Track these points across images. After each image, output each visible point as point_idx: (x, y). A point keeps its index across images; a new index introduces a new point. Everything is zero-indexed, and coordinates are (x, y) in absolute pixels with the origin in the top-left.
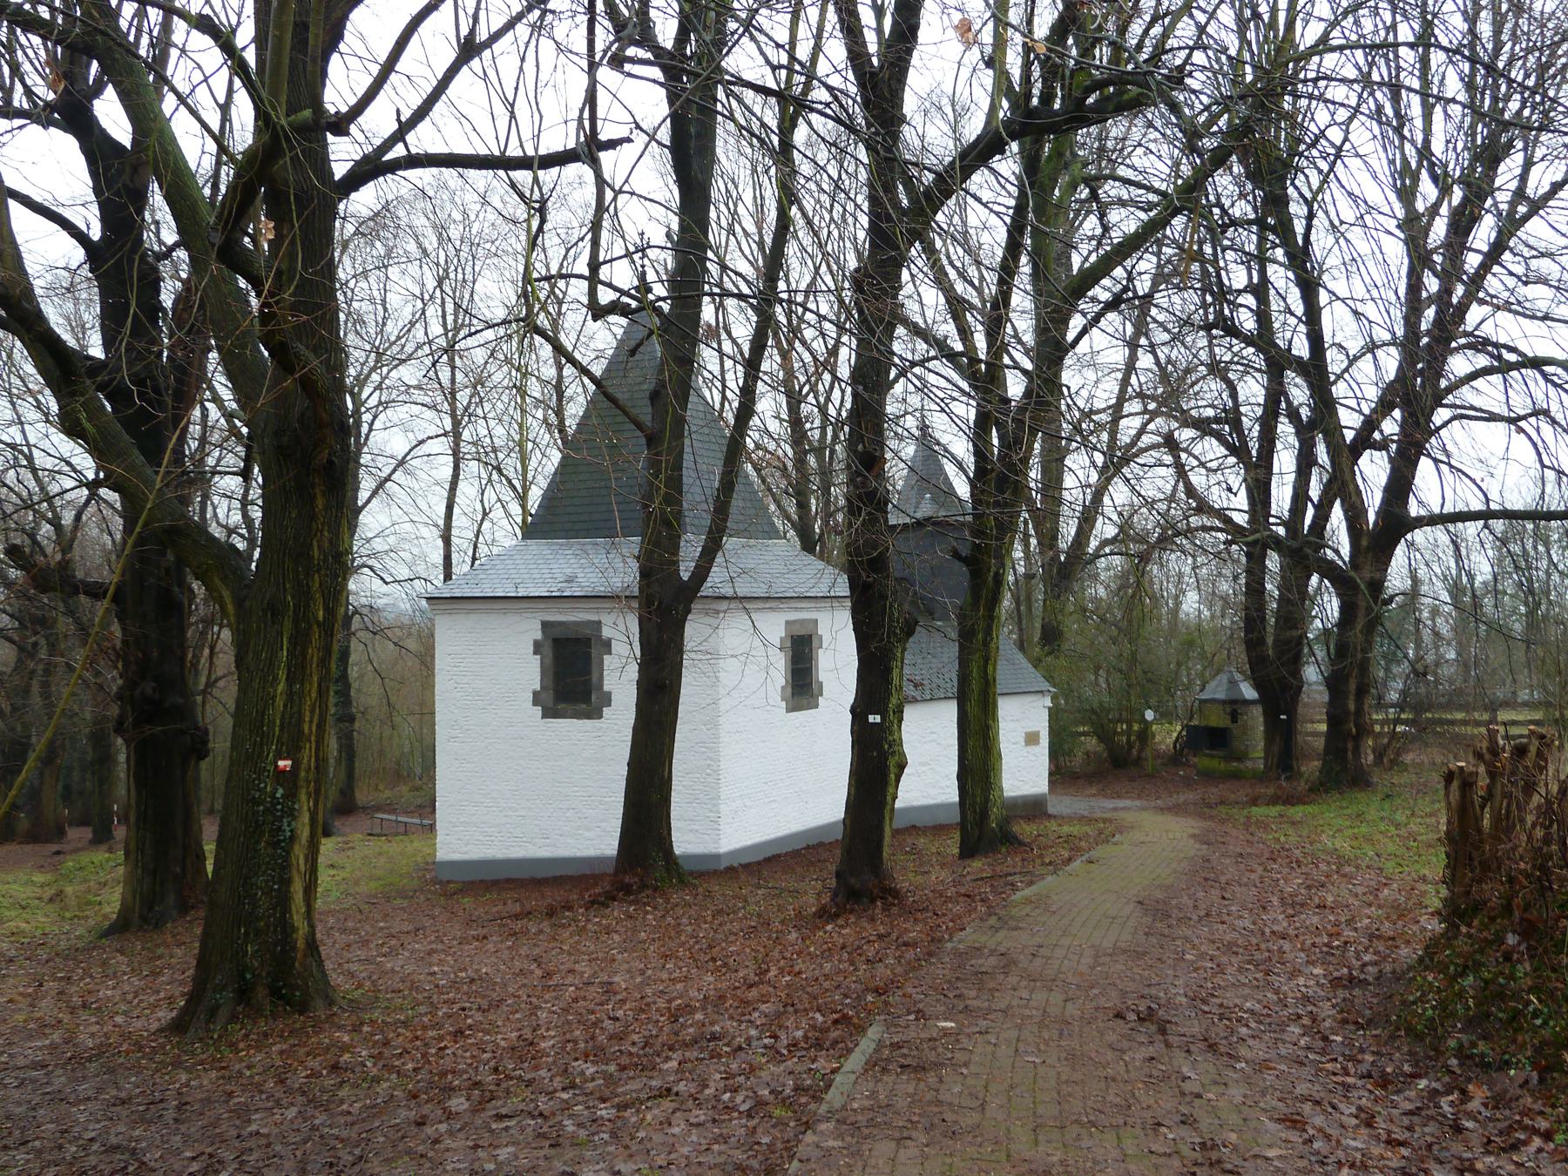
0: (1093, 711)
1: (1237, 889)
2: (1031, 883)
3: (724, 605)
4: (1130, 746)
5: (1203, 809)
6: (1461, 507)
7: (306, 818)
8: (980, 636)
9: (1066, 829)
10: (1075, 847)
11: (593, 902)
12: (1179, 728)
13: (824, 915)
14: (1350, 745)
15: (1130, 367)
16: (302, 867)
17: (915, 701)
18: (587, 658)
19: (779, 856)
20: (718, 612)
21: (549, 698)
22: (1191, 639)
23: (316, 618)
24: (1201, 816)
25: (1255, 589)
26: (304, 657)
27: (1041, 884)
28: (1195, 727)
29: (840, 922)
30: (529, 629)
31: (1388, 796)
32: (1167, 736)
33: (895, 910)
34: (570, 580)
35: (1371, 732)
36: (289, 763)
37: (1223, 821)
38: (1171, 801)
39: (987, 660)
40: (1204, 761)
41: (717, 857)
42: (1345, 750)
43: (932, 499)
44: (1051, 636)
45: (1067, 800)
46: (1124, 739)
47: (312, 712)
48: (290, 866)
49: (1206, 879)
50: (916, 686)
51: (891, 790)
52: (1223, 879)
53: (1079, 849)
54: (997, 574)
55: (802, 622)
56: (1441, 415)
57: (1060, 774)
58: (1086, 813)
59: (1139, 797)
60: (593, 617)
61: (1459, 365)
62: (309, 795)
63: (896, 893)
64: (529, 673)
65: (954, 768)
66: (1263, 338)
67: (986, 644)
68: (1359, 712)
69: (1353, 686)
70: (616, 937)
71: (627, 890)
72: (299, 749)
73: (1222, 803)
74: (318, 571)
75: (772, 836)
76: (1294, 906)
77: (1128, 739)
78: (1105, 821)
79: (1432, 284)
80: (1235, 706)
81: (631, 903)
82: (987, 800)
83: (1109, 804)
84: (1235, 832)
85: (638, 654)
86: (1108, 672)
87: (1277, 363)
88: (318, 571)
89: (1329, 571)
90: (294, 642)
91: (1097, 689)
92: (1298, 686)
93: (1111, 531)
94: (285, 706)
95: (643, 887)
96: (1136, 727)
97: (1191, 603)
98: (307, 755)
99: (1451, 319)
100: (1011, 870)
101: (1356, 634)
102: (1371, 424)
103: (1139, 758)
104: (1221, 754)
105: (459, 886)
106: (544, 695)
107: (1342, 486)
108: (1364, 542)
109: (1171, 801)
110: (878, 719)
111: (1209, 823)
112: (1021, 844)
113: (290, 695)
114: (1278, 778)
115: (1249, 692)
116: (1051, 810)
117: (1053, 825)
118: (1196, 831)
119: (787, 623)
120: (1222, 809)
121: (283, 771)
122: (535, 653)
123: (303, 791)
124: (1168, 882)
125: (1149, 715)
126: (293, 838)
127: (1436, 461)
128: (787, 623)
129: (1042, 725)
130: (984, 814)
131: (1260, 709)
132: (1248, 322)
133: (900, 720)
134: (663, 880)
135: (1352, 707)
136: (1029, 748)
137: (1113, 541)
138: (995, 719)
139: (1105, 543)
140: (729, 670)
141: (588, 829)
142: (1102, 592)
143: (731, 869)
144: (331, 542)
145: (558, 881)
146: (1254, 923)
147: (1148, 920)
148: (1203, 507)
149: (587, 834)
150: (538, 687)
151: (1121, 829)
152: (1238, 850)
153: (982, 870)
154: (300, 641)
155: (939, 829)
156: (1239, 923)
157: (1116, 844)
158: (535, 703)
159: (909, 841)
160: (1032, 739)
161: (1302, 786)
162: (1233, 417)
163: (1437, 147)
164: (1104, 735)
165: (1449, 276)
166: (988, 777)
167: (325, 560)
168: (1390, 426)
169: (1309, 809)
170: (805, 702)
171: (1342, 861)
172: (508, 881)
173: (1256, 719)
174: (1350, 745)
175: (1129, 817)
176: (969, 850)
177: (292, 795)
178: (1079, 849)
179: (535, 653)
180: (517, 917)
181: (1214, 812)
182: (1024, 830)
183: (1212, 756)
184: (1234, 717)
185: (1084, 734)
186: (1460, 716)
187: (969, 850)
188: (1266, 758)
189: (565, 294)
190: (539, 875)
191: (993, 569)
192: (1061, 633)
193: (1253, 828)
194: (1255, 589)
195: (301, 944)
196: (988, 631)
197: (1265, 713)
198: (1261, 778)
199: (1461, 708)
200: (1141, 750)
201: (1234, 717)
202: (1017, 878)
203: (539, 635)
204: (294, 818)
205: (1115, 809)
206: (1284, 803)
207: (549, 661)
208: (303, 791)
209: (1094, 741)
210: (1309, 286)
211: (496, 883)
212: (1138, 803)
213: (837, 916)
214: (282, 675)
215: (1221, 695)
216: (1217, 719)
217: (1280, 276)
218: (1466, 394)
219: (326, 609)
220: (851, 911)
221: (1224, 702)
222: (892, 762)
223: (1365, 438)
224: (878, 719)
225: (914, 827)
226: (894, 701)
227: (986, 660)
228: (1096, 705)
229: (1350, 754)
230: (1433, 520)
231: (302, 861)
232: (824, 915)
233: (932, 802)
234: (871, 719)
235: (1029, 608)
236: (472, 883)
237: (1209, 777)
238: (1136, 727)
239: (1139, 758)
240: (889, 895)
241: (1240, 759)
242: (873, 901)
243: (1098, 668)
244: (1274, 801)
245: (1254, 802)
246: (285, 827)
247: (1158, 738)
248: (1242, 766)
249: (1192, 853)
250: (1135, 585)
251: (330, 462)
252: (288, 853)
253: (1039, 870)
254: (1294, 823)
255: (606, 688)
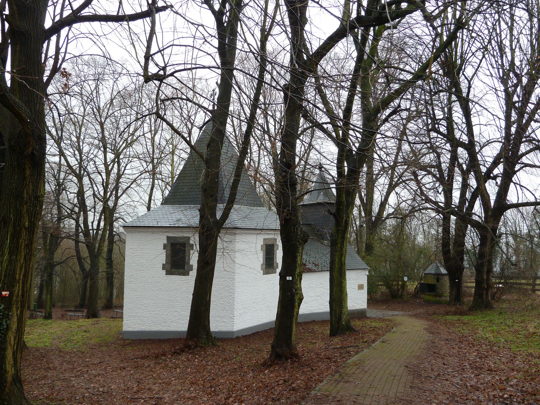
0: (384, 277)
1: (449, 358)
2: (357, 353)
3: (238, 231)
4: (398, 290)
5: (427, 316)
6: (525, 201)
7: (15, 319)
8: (339, 245)
9: (373, 324)
10: (377, 334)
11: (175, 353)
12: (417, 284)
13: (266, 365)
14: (484, 292)
15: (399, 149)
16: (12, 343)
17: (310, 271)
18: (184, 251)
19: (258, 332)
20: (235, 234)
21: (168, 267)
22: (422, 251)
23: (24, 226)
24: (427, 319)
25: (446, 230)
26: (18, 244)
27: (361, 354)
28: (423, 283)
29: (272, 369)
30: (161, 240)
31: (501, 313)
32: (412, 286)
33: (296, 364)
34: (178, 220)
35: (493, 287)
36: (8, 293)
37: (436, 322)
38: (414, 312)
39: (342, 255)
40: (427, 297)
41: (232, 333)
42: (482, 294)
43: (323, 194)
44: (369, 248)
45: (374, 311)
46: (396, 287)
47: (21, 269)
48: (6, 341)
49: (435, 353)
50: (316, 265)
51: (296, 310)
52: (442, 352)
53: (378, 335)
54: (346, 220)
55: (270, 239)
56: (517, 167)
57: (372, 300)
58: (381, 317)
59: (402, 310)
60: (186, 235)
61: (523, 148)
62: (17, 309)
63: (297, 356)
64: (162, 257)
65: (328, 298)
66: (450, 137)
67: (341, 249)
68: (488, 279)
69: (485, 269)
70: (178, 370)
71: (189, 347)
72: (13, 286)
73: (434, 314)
74: (26, 203)
75: (256, 324)
76: (477, 369)
77: (398, 287)
78: (389, 320)
79: (514, 116)
80: (438, 276)
81: (190, 353)
82: (341, 313)
83: (390, 313)
84: (441, 327)
85: (198, 250)
86: (390, 262)
87: (455, 144)
88: (26, 203)
89: (476, 225)
90: (13, 237)
91: (386, 268)
92: (461, 269)
93: (391, 211)
94: (7, 266)
95: (196, 346)
96: (400, 283)
97: (420, 239)
98: (18, 289)
99: (522, 129)
100: (350, 344)
101: (487, 249)
102: (490, 170)
103: (402, 295)
104: (433, 294)
105: (130, 342)
106: (167, 266)
107: (481, 192)
108: (490, 213)
109: (414, 312)
110: (291, 278)
111: (430, 323)
112: (355, 331)
113: (10, 261)
114: (456, 305)
115: (443, 271)
116: (368, 315)
117: (368, 322)
118: (426, 327)
119: (264, 239)
120: (435, 316)
121: (5, 297)
122: (164, 249)
123: (15, 306)
124: (418, 354)
125: (406, 279)
126: (8, 328)
127: (515, 183)
128: (264, 239)
129: (365, 282)
130: (340, 319)
131: (448, 277)
132: (443, 129)
133: (301, 279)
134: (205, 344)
135: (485, 277)
136: (360, 291)
137: (392, 214)
138: (345, 279)
139: (389, 215)
140: (239, 258)
141: (182, 320)
142: (388, 234)
143: (238, 338)
144: (33, 190)
145: (168, 341)
146: (461, 380)
147: (410, 377)
148: (428, 200)
149: (182, 322)
150: (164, 262)
151: (396, 325)
152: (446, 337)
153: (337, 343)
154: (16, 236)
155: (323, 322)
156: (455, 380)
157: (394, 332)
158: (163, 269)
159: (311, 327)
160: (361, 287)
161: (465, 308)
162: (439, 166)
163: (517, 63)
164: (389, 286)
165: (521, 115)
166: (342, 303)
167: (30, 199)
168: (499, 170)
169: (470, 317)
170: (271, 271)
171: (491, 344)
172: (150, 340)
173: (446, 281)
174: (484, 292)
175: (398, 319)
176: (334, 333)
177: (9, 307)
178: (378, 335)
179: (164, 249)
180: (144, 358)
181: (432, 318)
182: (356, 324)
183: (429, 295)
184: (438, 280)
185: (381, 285)
186: (524, 281)
187: (334, 333)
188: (450, 296)
189: (194, 121)
190: (161, 338)
191: (345, 218)
192: (373, 247)
193: (448, 325)
194: (446, 230)
195: (9, 379)
196: (342, 243)
197: (450, 279)
198: (449, 304)
199: (524, 278)
200: (402, 292)
201: (438, 280)
202: (351, 349)
203: (165, 241)
204: (9, 319)
205: (393, 315)
206: (459, 315)
207: (169, 252)
208: (15, 306)
209: (385, 288)
210: (467, 114)
211: (145, 340)
212: (401, 313)
213: (271, 366)
214: (6, 251)
215: (433, 272)
216: (431, 281)
217: (457, 109)
218: (524, 160)
219: (30, 221)
220: (277, 364)
221: (434, 275)
222: (297, 298)
223: (488, 175)
224: (291, 278)
225: (314, 321)
226: (298, 271)
227: (342, 255)
228: (385, 275)
229: (484, 295)
230: (517, 206)
231: (12, 339)
232: (266, 365)
233: (321, 311)
234: (288, 278)
235: (361, 238)
236: (136, 340)
237: (428, 303)
238: (400, 283)
239: (402, 295)
240: (294, 356)
241: (440, 296)
242: (287, 359)
243: (386, 261)
244: (455, 313)
245: (447, 314)
246: (4, 323)
247: (409, 288)
248: (441, 299)
249: (427, 338)
250: (400, 229)
251: (33, 154)
252: (5, 336)
253: (362, 345)
254: (464, 324)
255: (191, 263)
